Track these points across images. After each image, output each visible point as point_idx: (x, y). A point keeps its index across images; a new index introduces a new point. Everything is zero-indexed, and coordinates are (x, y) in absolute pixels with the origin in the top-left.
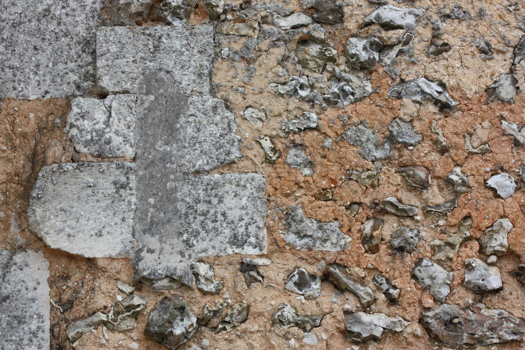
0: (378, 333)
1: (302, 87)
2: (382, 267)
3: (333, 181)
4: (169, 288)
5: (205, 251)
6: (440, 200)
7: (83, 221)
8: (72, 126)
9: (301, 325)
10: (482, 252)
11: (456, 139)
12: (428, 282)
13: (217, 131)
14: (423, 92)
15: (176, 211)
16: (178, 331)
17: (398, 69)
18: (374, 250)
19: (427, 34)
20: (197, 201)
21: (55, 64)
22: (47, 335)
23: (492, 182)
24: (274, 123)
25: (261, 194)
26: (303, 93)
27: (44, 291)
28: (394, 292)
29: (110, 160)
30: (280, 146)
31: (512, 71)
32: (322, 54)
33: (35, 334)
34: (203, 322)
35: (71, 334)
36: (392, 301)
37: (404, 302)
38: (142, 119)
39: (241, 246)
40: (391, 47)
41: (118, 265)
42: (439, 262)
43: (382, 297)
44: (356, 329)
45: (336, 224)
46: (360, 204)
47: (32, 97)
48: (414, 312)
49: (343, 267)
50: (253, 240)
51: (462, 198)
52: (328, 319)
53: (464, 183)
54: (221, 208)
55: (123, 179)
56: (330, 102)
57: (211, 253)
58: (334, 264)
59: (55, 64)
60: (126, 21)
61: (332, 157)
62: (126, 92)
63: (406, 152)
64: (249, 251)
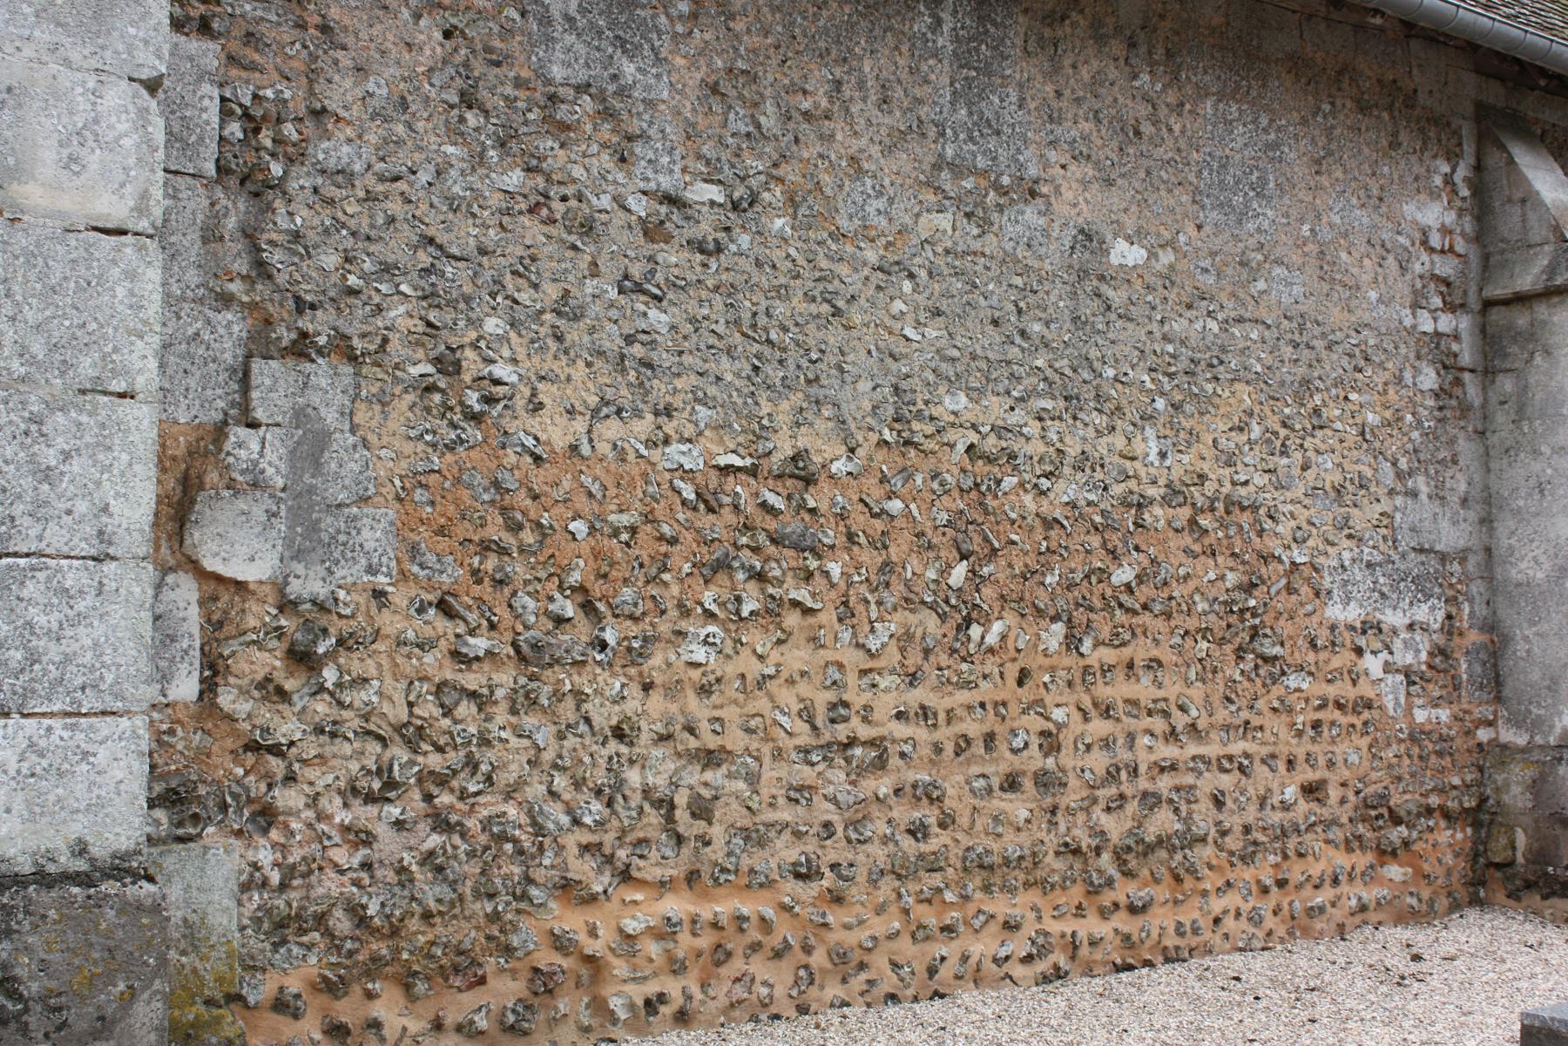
0: (481, 654)
1: (427, 432)
2: (485, 598)
3: (450, 519)
4: (310, 612)
5: (344, 578)
6: (531, 541)
7: (237, 546)
8: (228, 454)
9: (420, 646)
10: (561, 588)
11: (545, 488)
12: (520, 610)
13: (356, 467)
14: (523, 445)
15: (320, 541)
16: (321, 650)
17: (503, 422)
18: (479, 582)
19: (527, 392)
20: (339, 532)
21: (204, 389)
22: (197, 653)
23: (571, 527)
24: (404, 464)
25: (393, 529)
26: (428, 438)
27: (194, 612)
28: (495, 619)
29: (264, 489)
30: (408, 485)
31: (589, 432)
32: (444, 403)
33: (186, 652)
34: (341, 642)
35: (226, 653)
36: (492, 626)
37: (502, 627)
38: (292, 452)
39: (375, 574)
40: (498, 401)
41: (267, 589)
42: (529, 594)
43: (485, 623)
44: (464, 650)
45: (451, 558)
46: (470, 541)
47: (182, 421)
48: (509, 636)
49: (455, 596)
50: (384, 569)
51: (548, 540)
52: (443, 642)
53: (551, 527)
54: (359, 540)
55: (275, 508)
56: (450, 448)
57: (349, 580)
58: (449, 593)
59: (204, 389)
60: (275, 354)
61: (449, 497)
62: (278, 425)
63: (507, 497)
64: (382, 579)
